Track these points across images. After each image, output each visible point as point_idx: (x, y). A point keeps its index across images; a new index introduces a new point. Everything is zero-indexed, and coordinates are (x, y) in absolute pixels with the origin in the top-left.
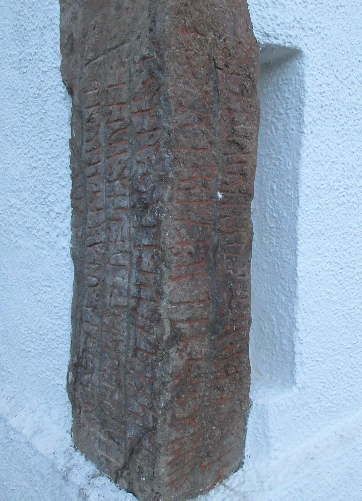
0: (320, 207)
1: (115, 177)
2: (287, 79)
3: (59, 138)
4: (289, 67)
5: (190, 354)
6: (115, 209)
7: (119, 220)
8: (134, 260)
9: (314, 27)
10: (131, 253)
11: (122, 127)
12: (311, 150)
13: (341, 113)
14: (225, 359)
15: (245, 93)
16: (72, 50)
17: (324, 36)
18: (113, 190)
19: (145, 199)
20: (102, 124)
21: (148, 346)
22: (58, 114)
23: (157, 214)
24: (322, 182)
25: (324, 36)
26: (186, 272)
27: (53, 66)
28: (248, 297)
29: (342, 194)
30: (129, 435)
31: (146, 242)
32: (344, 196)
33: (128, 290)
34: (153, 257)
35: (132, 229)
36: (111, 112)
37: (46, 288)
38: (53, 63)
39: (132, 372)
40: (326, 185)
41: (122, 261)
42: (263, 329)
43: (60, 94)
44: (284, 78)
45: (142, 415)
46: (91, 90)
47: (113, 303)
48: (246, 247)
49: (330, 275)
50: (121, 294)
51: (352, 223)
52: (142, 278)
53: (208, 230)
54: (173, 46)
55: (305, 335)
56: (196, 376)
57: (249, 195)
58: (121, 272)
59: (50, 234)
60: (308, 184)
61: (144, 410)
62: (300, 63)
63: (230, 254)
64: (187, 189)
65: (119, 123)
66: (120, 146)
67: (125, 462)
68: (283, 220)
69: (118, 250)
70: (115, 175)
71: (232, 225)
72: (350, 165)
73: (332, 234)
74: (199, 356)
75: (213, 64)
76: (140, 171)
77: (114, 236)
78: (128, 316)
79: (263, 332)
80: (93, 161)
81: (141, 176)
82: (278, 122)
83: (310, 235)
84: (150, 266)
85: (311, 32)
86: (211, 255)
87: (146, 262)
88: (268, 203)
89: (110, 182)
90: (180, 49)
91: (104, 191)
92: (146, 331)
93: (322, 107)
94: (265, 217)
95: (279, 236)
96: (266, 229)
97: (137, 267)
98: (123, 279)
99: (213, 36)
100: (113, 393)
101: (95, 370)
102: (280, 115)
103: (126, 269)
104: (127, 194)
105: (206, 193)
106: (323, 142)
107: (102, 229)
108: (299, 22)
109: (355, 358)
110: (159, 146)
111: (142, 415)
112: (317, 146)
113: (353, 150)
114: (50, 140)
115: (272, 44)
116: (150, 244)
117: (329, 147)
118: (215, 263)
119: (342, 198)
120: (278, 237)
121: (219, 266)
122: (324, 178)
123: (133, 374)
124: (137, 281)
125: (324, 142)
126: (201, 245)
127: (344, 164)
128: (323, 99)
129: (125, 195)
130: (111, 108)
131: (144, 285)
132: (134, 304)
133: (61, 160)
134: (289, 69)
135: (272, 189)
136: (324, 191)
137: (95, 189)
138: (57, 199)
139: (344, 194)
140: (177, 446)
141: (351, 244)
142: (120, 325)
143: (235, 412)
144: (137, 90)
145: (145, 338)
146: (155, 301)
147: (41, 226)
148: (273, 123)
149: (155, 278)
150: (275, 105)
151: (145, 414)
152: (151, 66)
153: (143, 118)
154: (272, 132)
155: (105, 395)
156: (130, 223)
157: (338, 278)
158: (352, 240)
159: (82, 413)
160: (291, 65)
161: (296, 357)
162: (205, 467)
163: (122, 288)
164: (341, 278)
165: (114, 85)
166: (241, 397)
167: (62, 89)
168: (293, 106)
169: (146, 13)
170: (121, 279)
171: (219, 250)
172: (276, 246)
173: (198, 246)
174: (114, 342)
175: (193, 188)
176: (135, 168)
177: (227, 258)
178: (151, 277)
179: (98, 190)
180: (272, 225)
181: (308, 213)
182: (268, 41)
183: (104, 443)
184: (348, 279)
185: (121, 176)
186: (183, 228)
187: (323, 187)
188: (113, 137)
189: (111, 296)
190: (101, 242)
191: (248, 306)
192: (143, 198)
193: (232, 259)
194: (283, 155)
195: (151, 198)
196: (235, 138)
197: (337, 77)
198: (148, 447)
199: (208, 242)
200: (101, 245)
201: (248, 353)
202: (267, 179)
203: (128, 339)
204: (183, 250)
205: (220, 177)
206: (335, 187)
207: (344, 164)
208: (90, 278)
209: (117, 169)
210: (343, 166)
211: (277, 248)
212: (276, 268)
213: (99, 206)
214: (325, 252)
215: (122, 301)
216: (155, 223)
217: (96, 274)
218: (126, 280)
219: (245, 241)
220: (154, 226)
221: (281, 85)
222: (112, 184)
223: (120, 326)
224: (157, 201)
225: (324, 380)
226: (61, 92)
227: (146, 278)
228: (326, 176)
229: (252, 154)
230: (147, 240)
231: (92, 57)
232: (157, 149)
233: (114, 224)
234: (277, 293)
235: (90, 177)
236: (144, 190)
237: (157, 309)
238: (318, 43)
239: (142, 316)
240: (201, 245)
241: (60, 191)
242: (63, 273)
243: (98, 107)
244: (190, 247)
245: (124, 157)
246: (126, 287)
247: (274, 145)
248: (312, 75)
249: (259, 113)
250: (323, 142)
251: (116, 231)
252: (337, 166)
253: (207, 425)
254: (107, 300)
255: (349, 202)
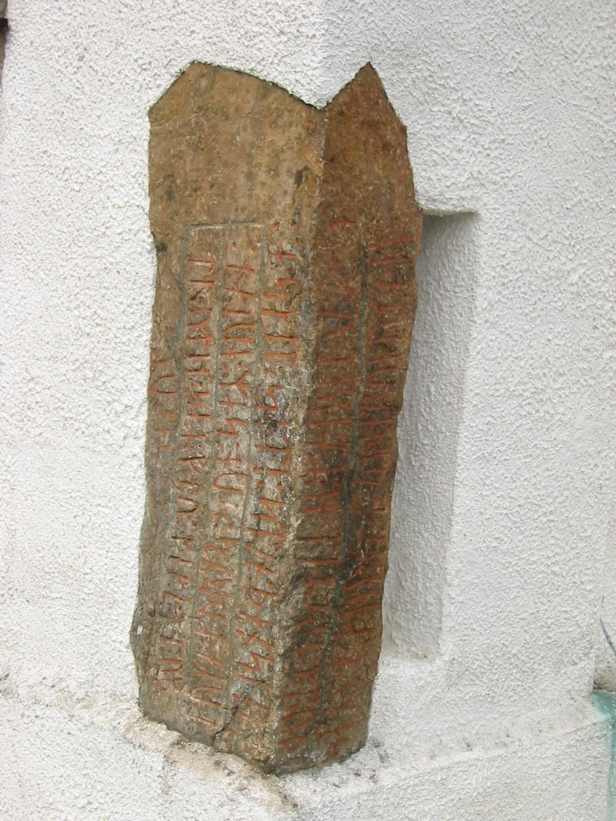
0: (493, 421)
1: (232, 381)
2: (458, 246)
3: (136, 302)
4: (461, 229)
5: (314, 598)
6: (228, 420)
7: (233, 433)
8: (254, 485)
9: (498, 179)
10: (249, 476)
11: (247, 322)
12: (484, 346)
13: (533, 288)
14: (353, 610)
15: (400, 280)
16: (170, 195)
17: (513, 188)
18: (227, 395)
19: (274, 416)
20: (216, 309)
21: (267, 585)
22: (136, 269)
23: (288, 436)
24: (498, 387)
25: (513, 188)
26: (317, 504)
27: (133, 201)
28: (386, 538)
29: (527, 401)
30: (233, 691)
31: (272, 465)
32: (529, 404)
33: (243, 521)
34: (280, 484)
35: (253, 448)
36: (231, 299)
37: (99, 508)
38: (134, 199)
39: (242, 616)
40: (502, 391)
41: (235, 484)
42: (403, 583)
43: (143, 244)
44: (454, 242)
45: (253, 665)
46: (201, 261)
47: (219, 534)
48: (388, 473)
49: (501, 514)
50: (231, 525)
51: (541, 443)
52: (263, 507)
53: (344, 455)
54: (320, 244)
55: (459, 592)
56: (319, 626)
57: (396, 407)
58: (234, 497)
59: (112, 433)
60: (477, 391)
61: (256, 660)
62: (476, 228)
63: (367, 483)
64: (324, 408)
65: (241, 315)
66: (242, 345)
67: (225, 724)
68: (440, 435)
69: (231, 470)
70: (231, 378)
71: (373, 446)
72: (544, 359)
73: (507, 458)
74: (325, 602)
75: (363, 253)
76: (269, 380)
77: (225, 453)
78: (240, 551)
79: (403, 587)
80: (197, 353)
81: (269, 387)
82: (442, 299)
83: (475, 459)
84: (275, 494)
85: (492, 187)
86: (345, 484)
87: (270, 489)
88: (423, 410)
89: (222, 384)
90: (327, 246)
91: (213, 393)
92: (267, 569)
93: (504, 284)
94: (417, 429)
95: (434, 457)
96: (416, 446)
97: (257, 493)
98: (237, 506)
99: (364, 220)
100: (212, 643)
101: (186, 617)
102: (446, 291)
103: (242, 494)
104: (249, 404)
105: (345, 410)
106: (502, 332)
107: (207, 441)
108: (476, 179)
109: (533, 634)
110: (296, 357)
111: (253, 665)
112: (493, 338)
113: (550, 337)
114: (121, 303)
115: (439, 211)
116: (277, 468)
117: (512, 338)
118: (349, 493)
119: (527, 408)
120: (432, 459)
121: (354, 498)
122: (502, 381)
123: (243, 619)
124: (257, 510)
125: (504, 331)
126: (334, 472)
127: (533, 358)
128: (506, 273)
129: (245, 404)
130: (231, 293)
131: (266, 515)
132: (251, 538)
133: (136, 334)
134: (462, 232)
135: (429, 392)
136: (500, 399)
137: (200, 388)
138: (127, 386)
139: (530, 400)
140: (293, 701)
141: (538, 471)
142: (228, 561)
143: (359, 679)
144: (271, 285)
145: (265, 576)
146: (279, 535)
147: (94, 418)
148: (437, 300)
149: (281, 509)
150: (440, 276)
151: (258, 664)
152: (291, 266)
153: (277, 321)
154: (434, 313)
155: (200, 648)
156: (250, 440)
157: (513, 519)
158: (537, 467)
159: (160, 673)
160: (464, 228)
161: (443, 619)
162: (321, 735)
163: (234, 516)
164: (517, 519)
165: (236, 266)
166: (368, 662)
167: (146, 239)
168: (463, 283)
169: (289, 200)
170: (233, 507)
171: (355, 477)
172: (429, 470)
173: (331, 473)
174: (217, 582)
175: (331, 406)
176: (262, 376)
177: (364, 488)
178: (276, 506)
179: (204, 391)
180: (425, 442)
181: (474, 429)
182: (433, 207)
183: (196, 704)
184: (529, 521)
185: (239, 380)
186: (317, 453)
187: (498, 394)
188: (230, 330)
189: (216, 526)
190: (204, 457)
191: (384, 548)
192: (271, 414)
193: (369, 489)
194: (446, 346)
195: (282, 415)
196: (383, 340)
197: (529, 239)
198: (259, 701)
199: (343, 469)
200: (203, 461)
201: (380, 608)
202: (423, 376)
203: (239, 578)
204: (315, 478)
205: (362, 389)
206: (517, 393)
207: (533, 358)
208: (182, 501)
209: (234, 371)
210: (531, 362)
211: (430, 474)
212: (427, 500)
213: (203, 411)
214: (496, 482)
215: (234, 533)
216: (286, 445)
217: (194, 497)
218: (241, 508)
219: (386, 466)
220: (284, 448)
221: (450, 251)
222: (226, 388)
223: (228, 564)
224: (290, 421)
225: (481, 658)
226: (144, 241)
227: (268, 507)
228: (504, 378)
229: (403, 356)
230: (273, 463)
231: (205, 220)
232: (293, 361)
233: (226, 438)
234: (426, 535)
235: (190, 371)
236: (274, 405)
237: (282, 543)
238: (503, 198)
239: (262, 551)
240: (334, 472)
241: (133, 376)
242: (131, 489)
243: (210, 284)
244: (324, 474)
245: (247, 359)
246: (241, 516)
247: (435, 331)
248: (492, 244)
249: (415, 301)
250: (502, 332)
251: (229, 446)
252: (522, 364)
253: (326, 685)
254: (210, 530)
255: (537, 411)
